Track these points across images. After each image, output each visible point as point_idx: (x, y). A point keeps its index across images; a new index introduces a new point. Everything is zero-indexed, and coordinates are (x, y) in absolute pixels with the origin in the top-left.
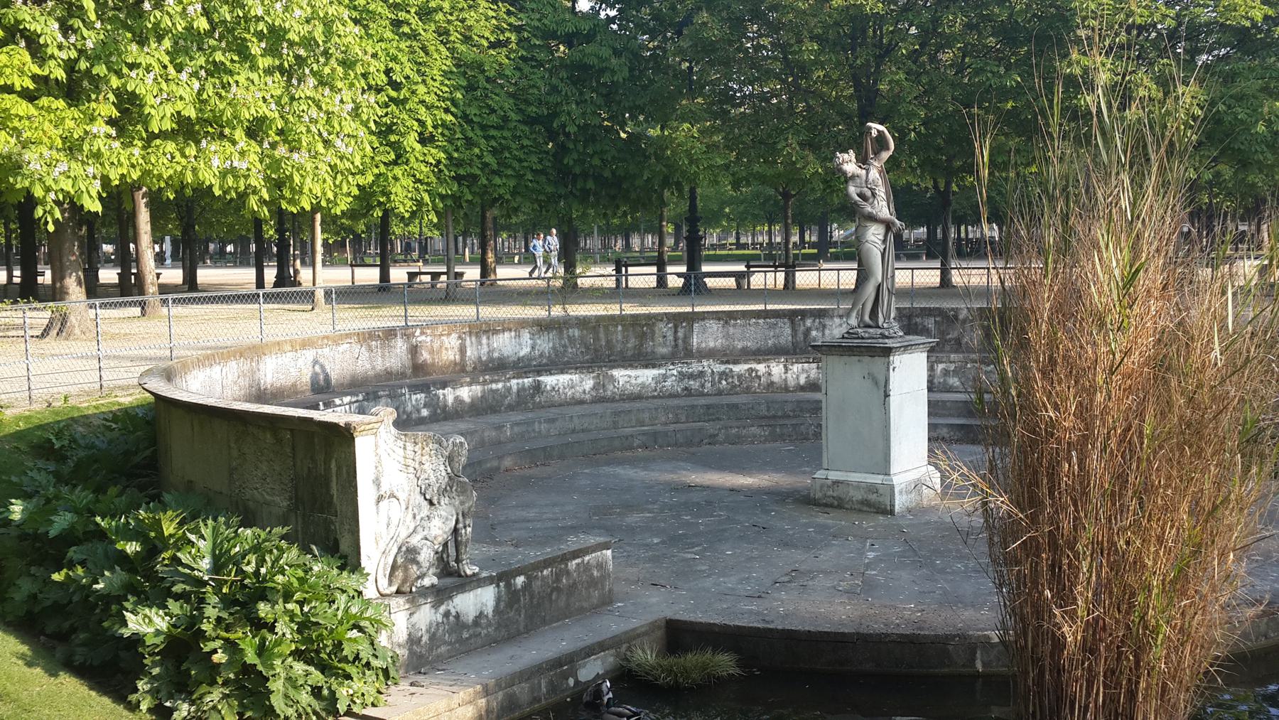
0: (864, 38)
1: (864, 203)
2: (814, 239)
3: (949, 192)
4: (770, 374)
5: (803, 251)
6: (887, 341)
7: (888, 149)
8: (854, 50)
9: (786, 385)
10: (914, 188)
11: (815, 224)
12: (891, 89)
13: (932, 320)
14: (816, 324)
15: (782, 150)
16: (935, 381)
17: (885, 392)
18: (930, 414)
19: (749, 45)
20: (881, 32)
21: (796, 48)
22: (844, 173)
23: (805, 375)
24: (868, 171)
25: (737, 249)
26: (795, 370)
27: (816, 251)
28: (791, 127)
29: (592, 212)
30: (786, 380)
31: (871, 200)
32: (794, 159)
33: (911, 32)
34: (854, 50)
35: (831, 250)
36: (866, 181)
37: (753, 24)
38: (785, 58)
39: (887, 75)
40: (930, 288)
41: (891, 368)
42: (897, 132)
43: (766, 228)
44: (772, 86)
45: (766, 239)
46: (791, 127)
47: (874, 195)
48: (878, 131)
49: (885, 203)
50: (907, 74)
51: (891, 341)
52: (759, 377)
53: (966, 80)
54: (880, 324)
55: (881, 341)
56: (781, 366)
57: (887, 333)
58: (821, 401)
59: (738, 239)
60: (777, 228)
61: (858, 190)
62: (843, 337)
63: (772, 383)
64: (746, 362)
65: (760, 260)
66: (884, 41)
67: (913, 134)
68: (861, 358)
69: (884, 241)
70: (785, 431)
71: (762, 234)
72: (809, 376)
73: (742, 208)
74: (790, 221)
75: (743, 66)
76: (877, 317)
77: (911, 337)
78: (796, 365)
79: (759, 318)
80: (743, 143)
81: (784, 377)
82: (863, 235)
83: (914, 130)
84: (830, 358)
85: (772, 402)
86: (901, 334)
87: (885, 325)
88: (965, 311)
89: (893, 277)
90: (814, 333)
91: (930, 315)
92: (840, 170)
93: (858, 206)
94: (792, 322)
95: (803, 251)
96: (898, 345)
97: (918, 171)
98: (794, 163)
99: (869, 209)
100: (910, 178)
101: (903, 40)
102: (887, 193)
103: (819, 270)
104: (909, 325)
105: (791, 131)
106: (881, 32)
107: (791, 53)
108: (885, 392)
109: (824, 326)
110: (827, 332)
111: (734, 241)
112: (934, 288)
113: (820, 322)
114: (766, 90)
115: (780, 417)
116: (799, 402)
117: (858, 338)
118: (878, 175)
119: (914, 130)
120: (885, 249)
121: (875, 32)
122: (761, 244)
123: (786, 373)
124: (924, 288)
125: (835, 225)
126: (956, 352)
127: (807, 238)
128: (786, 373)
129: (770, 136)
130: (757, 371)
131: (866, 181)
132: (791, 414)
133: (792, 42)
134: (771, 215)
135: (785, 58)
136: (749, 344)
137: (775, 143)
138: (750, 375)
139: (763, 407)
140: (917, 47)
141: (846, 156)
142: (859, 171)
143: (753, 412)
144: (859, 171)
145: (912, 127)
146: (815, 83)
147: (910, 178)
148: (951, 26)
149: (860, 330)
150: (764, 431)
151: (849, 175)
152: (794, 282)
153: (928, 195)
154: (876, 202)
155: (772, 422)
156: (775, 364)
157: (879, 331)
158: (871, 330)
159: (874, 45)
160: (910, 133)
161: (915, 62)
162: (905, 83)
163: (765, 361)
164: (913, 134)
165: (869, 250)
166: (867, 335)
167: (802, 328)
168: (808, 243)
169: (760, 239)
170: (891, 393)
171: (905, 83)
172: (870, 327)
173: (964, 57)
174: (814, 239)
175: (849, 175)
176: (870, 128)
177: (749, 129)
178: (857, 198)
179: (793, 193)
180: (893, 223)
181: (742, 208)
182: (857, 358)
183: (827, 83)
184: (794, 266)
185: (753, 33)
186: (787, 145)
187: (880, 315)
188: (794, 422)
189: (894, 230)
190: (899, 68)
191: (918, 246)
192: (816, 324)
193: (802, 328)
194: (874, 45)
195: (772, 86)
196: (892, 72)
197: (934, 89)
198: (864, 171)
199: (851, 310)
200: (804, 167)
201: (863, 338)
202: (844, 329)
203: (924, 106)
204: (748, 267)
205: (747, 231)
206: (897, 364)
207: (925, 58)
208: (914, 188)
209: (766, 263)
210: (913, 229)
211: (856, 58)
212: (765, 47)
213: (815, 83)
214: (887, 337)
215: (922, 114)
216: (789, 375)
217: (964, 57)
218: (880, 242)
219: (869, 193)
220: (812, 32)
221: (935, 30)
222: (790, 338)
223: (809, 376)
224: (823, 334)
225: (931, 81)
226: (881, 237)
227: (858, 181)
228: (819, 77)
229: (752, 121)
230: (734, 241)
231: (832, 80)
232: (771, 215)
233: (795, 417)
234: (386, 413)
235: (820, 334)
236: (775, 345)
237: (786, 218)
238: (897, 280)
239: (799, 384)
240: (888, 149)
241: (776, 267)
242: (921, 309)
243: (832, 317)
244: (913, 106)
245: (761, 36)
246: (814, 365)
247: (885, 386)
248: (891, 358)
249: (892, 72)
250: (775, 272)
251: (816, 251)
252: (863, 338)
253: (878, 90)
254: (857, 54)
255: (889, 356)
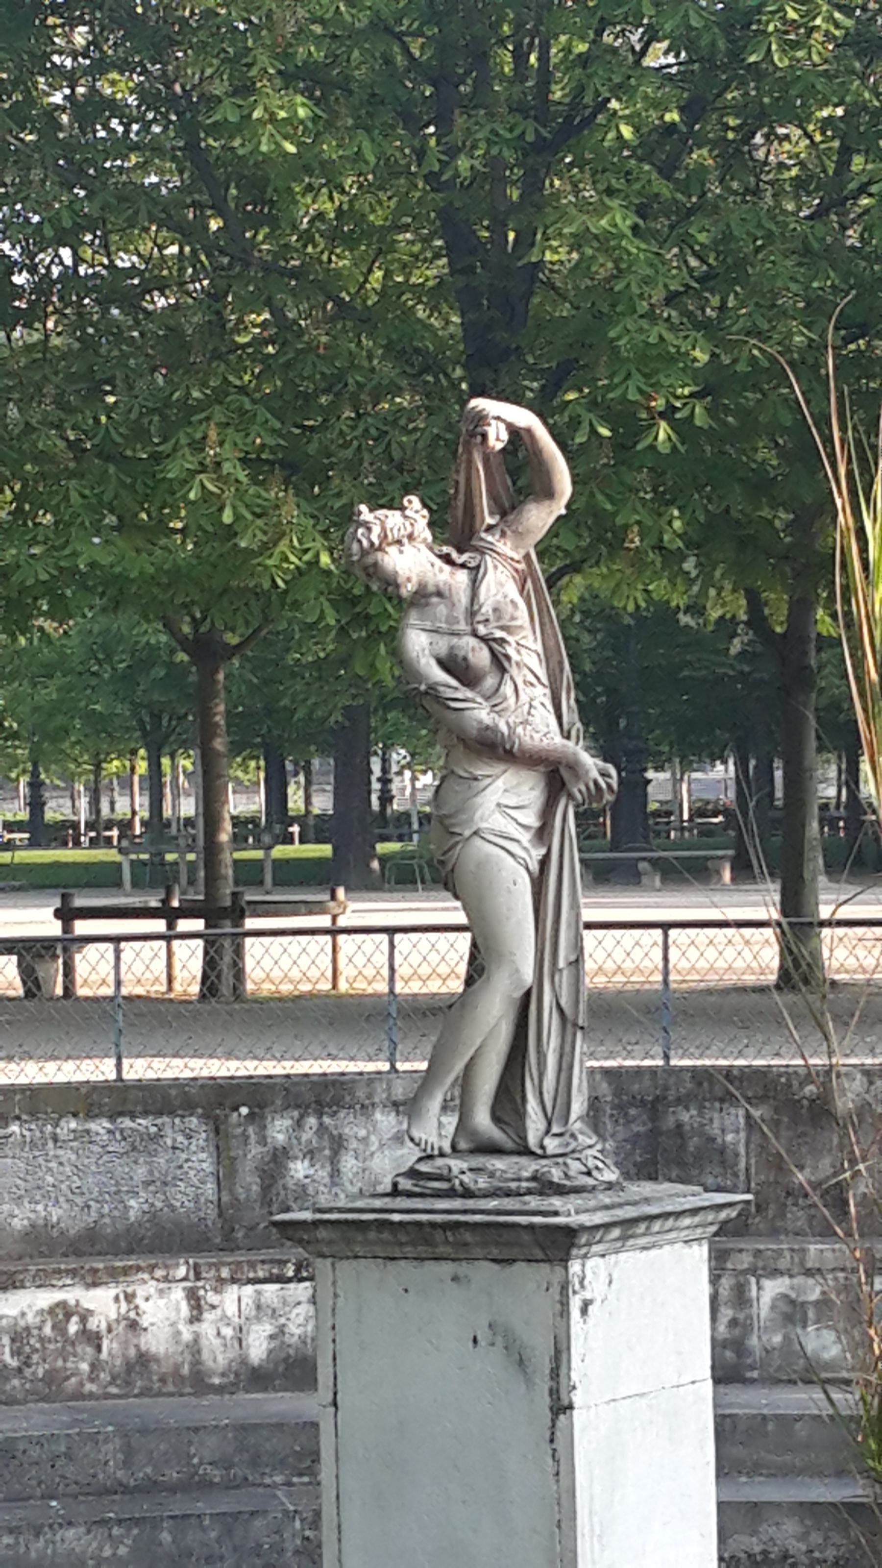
0: (482, 84)
1: (465, 693)
2: (323, 803)
3: (803, 640)
4: (133, 1325)
5: (280, 851)
6: (556, 1202)
7: (548, 493)
8: (443, 122)
9: (197, 1362)
10: (685, 619)
11: (322, 751)
12: (581, 268)
13: (737, 1116)
14: (307, 1135)
15: (186, 482)
16: (753, 1341)
17: (554, 1392)
18: (721, 1473)
19: (57, 98)
20: (544, 58)
21: (228, 113)
22: (390, 583)
23: (267, 1328)
24: (476, 574)
25: (33, 844)
26: (231, 1309)
27: (325, 850)
28: (218, 397)
29: (657, 122)
30: (195, 1347)
31: (490, 682)
32: (227, 517)
33: (649, 61)
34: (443, 122)
35: (382, 848)
36: (472, 613)
37: (73, 23)
38: (193, 148)
39: (563, 215)
40: (743, 990)
41: (575, 1304)
42: (605, 420)
43: (142, 767)
44: (146, 246)
45: (142, 803)
46: (218, 397)
47: (500, 663)
48: (515, 432)
49: (541, 694)
50: (642, 211)
51: (571, 1203)
52: (94, 1339)
53: (853, 237)
54: (532, 1140)
55: (534, 1202)
56: (178, 1294)
57: (556, 1175)
58: (315, 1425)
59: (36, 805)
60: (186, 763)
61: (443, 645)
62: (395, 1192)
63: (144, 1359)
64: (43, 1281)
65: (118, 884)
66: (557, 95)
67: (663, 430)
68: (463, 1268)
69: (542, 833)
70: (192, 1538)
71: (127, 785)
72: (281, 1330)
73: (49, 692)
74: (219, 744)
75: (36, 174)
76: (521, 1115)
77: (647, 1188)
78: (232, 1292)
79: (91, 1116)
80: (38, 457)
81: (187, 1335)
82: (465, 807)
83: (668, 413)
84: (344, 1266)
85: (144, 1431)
86: (611, 1175)
87: (552, 1145)
88: (858, 1083)
89: (577, 963)
90: (299, 1169)
91: (727, 1098)
92: (374, 571)
93: (442, 701)
94: (218, 1129)
95: (280, 851)
96: (599, 1218)
97: (689, 565)
98: (231, 532)
99: (482, 714)
100: (659, 588)
101: (620, 90)
102: (549, 656)
103: (334, 932)
104: (655, 1133)
105: (219, 414)
106: (544, 58)
107: (215, 130)
108: (554, 1392)
109: (338, 1144)
110: (349, 1163)
111: (24, 815)
112: (761, 990)
113: (322, 1129)
114: (124, 261)
115: (173, 1489)
116: (244, 1429)
117: (451, 1193)
118: (513, 591)
119: (668, 413)
120: (544, 862)
121: (520, 57)
122: (125, 826)
123: (196, 1319)
124: (726, 992)
125: (399, 755)
126: (827, 1233)
127: (295, 801)
128: (196, 1319)
129: (140, 434)
130: (85, 1316)
131: (472, 613)
132: (216, 1475)
133: (218, 89)
134: (156, 717)
135: (193, 148)
136: (55, 1214)
137: (157, 458)
138: (60, 1328)
139: (111, 1451)
140: (673, 116)
141: (393, 518)
142: (443, 575)
143: (70, 1471)
144: (443, 575)
145: (659, 404)
146: (307, 238)
147: (659, 588)
148: (795, 45)
149: (456, 1165)
150: (116, 1542)
151: (408, 589)
152: (239, 974)
153: (736, 646)
154: (508, 689)
155: (144, 1508)
156: (151, 1287)
157: (529, 1167)
158: (498, 1164)
159: (519, 109)
160: (652, 425)
161: (666, 171)
162: (632, 246)
163: (115, 1275)
164: (663, 430)
165: (484, 863)
166: (483, 1183)
167: (255, 1150)
168: (300, 820)
169: (122, 807)
170: (577, 1398)
171: (632, 246)
172: (495, 1150)
173: (845, 154)
174: (323, 803)
175: (408, 589)
176: (481, 418)
177: (60, 403)
178: (439, 675)
179: (233, 639)
180: (574, 767)
181: (49, 692)
182: (447, 1268)
183: (351, 243)
184: (238, 913)
185: (74, 55)
186: (203, 468)
187: (532, 1105)
188: (226, 1504)
189: (578, 789)
190: (610, 192)
191: (707, 832)
192: (307, 1135)
193: (255, 1150)
194: (519, 109)
195: (146, 246)
196: (583, 206)
197: (741, 264)
198: (462, 577)
199: (428, 1080)
200: (266, 548)
201: (468, 1193)
202: (409, 1155)
203: (705, 326)
204: (66, 915)
205: (70, 779)
206: (595, 1288)
207: (700, 156)
208: (685, 619)
209: (135, 901)
210: (687, 766)
211: (453, 152)
212: (113, 107)
213: (307, 238)
214: (561, 1190)
215: (702, 356)
216: (207, 1327)
217: (845, 154)
218: (525, 837)
219: (481, 657)
220: (286, 56)
221: (736, 55)
222: (210, 1188)
223: (281, 1330)
224: (335, 1173)
225: (728, 237)
226: (531, 818)
227: (442, 609)
228: (320, 216)
229: (71, 378)
230: (24, 815)
231: (370, 232)
232: (156, 717)
233: (230, 1485)
234: (104, 765)
235: (323, 1174)
236: (153, 1215)
237: (207, 731)
238: (589, 965)
239: (244, 1361)
240: (548, 493)
241: (171, 915)
242: (700, 1075)
243: (366, 1109)
244: (660, 329)
245: (100, 67)
246: (302, 1290)
247: (555, 1374)
248: (575, 1267)
249: (583, 206)
250: (167, 938)
251: (325, 850)
252: (468, 1193)
253: (539, 265)
254: (457, 137)
255: (565, 1261)
